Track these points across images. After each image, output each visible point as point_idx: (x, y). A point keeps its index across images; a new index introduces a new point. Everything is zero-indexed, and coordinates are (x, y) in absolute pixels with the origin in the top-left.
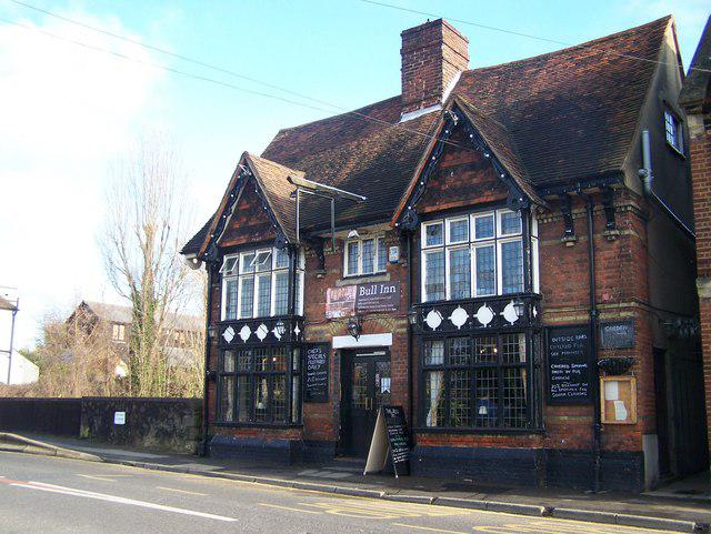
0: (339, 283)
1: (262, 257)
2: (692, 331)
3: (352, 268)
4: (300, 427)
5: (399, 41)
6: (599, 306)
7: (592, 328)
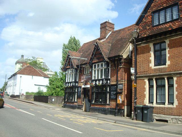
0: (83, 75)
1: (72, 70)
2: (69, 85)
3: (86, 73)
4: (77, 102)
5: (100, 26)
6: (118, 81)
7: (116, 85)
